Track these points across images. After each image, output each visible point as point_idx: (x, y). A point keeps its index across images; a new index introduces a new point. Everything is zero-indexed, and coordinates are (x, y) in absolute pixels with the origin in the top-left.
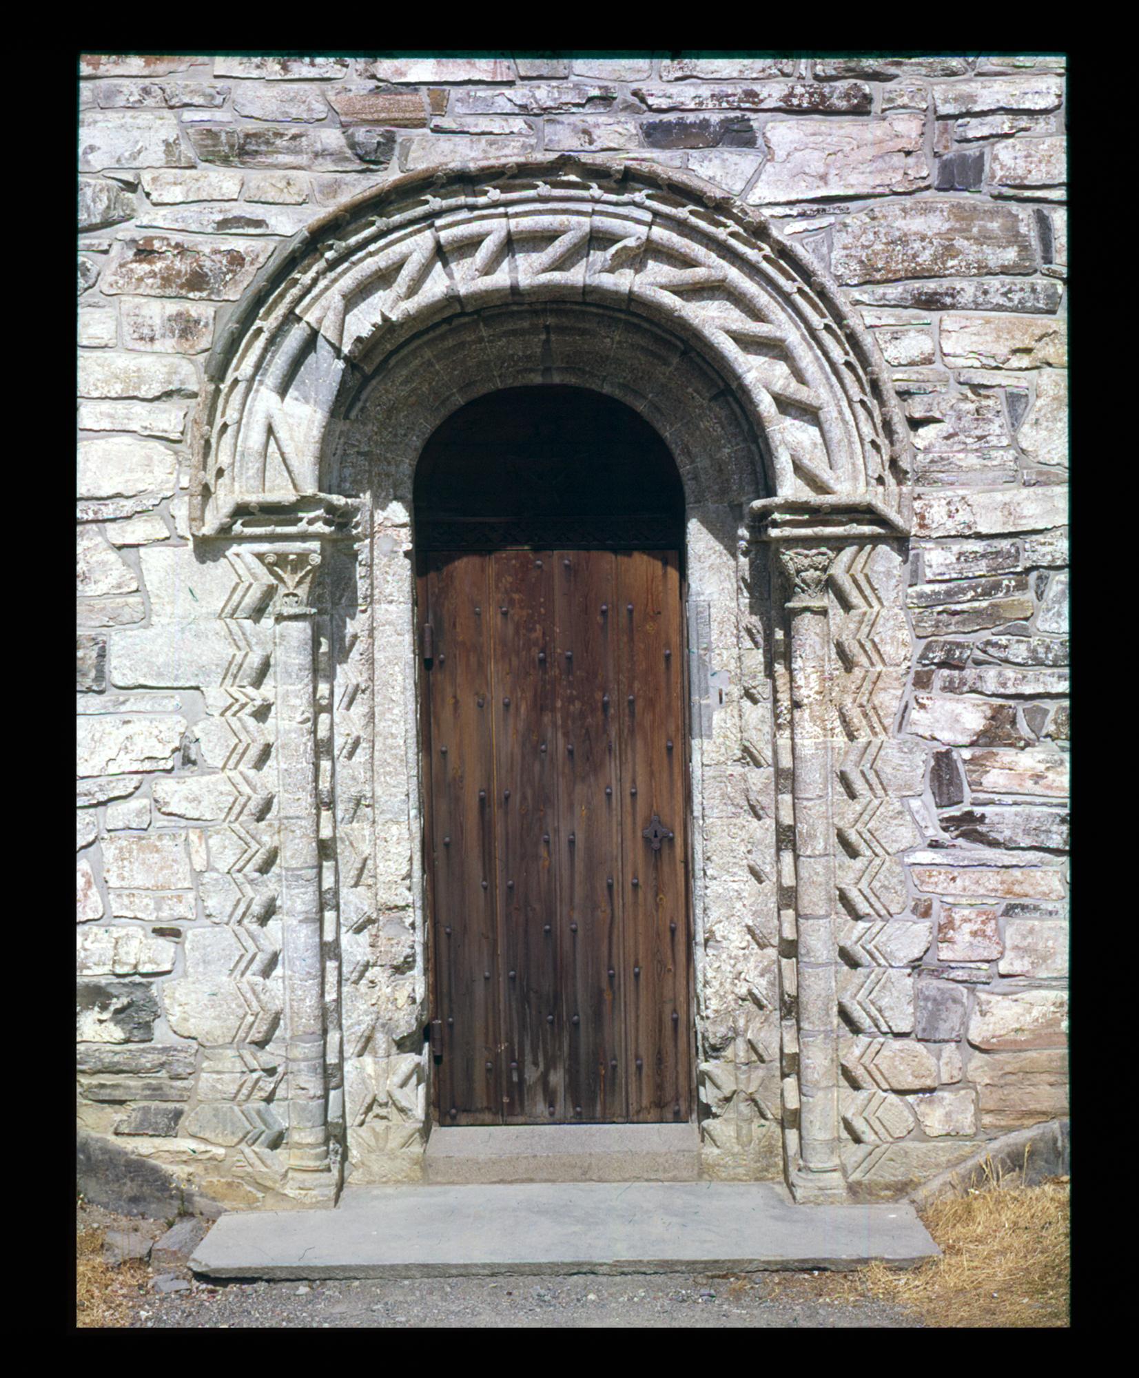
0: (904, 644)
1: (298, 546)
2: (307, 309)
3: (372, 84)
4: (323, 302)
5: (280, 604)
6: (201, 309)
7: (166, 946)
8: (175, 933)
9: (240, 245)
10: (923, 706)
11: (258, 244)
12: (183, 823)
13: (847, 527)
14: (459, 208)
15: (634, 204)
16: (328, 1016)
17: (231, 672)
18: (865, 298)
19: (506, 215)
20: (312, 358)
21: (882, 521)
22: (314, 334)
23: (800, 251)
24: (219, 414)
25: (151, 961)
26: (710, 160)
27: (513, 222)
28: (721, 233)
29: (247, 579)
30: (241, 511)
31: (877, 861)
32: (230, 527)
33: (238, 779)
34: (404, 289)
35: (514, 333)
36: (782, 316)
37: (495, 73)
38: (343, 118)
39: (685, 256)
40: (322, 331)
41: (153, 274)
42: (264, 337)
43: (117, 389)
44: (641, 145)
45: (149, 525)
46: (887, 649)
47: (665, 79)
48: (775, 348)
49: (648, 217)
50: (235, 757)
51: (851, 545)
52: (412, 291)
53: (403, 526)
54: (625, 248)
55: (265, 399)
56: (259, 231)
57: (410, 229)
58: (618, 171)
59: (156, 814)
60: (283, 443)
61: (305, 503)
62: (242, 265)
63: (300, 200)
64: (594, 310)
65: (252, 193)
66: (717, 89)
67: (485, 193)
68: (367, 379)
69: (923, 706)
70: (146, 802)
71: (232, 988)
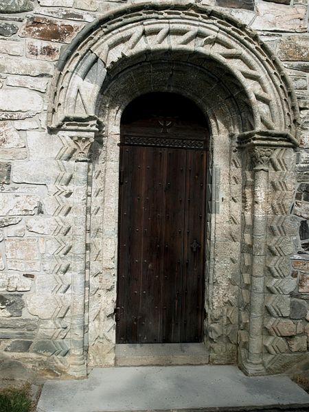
0: (294, 184)
2: (96, 48)
5: (76, 156)
6: (55, 45)
7: (28, 280)
8: (32, 276)
9: (72, 24)
10: (298, 205)
12: (37, 235)
15: (213, 24)
16: (86, 307)
17: (58, 179)
19: (169, 23)
20: (95, 65)
21: (290, 140)
22: (97, 58)
23: (269, 46)
24: (67, 65)
25: (22, 286)
28: (242, 37)
29: (66, 145)
30: (67, 119)
31: (282, 258)
33: (58, 219)
39: (227, 44)
41: (38, 31)
42: (80, 56)
43: (22, 71)
45: (31, 123)
46: (289, 185)
48: (255, 78)
49: (217, 29)
50: (58, 211)
55: (77, 80)
56: (80, 19)
57: (134, 24)
59: (27, 232)
60: (83, 97)
61: (91, 118)
64: (189, 65)
69: (298, 205)
70: (22, 227)
71: (51, 297)
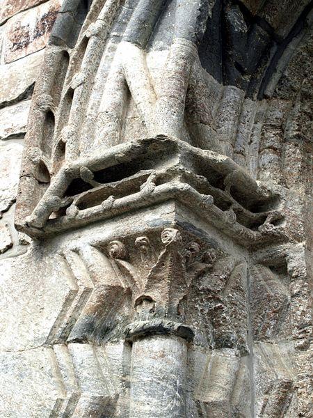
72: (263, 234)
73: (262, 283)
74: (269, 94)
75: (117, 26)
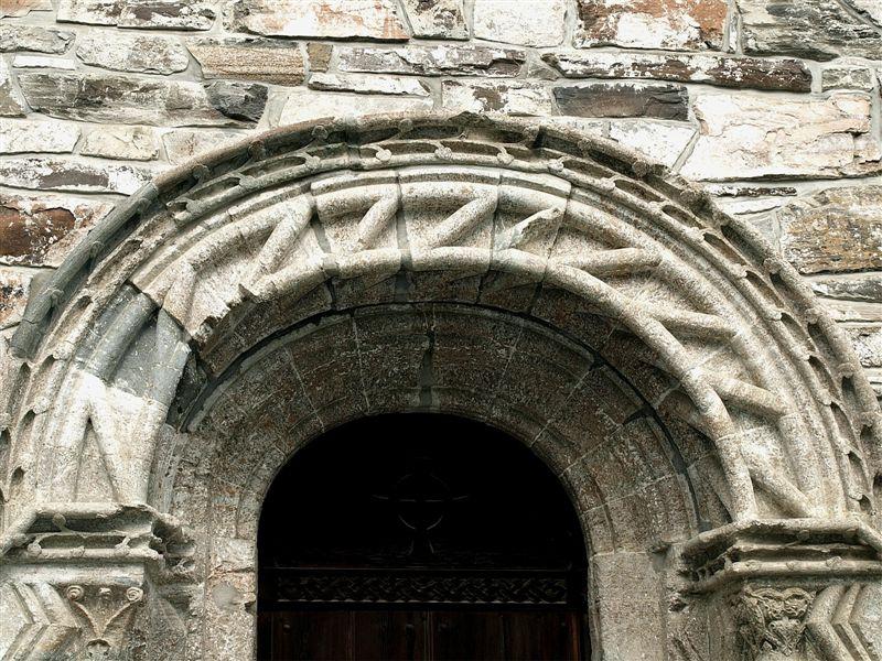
1: (115, 575)
3: (243, 37)
4: (168, 271)
9: (71, 203)
11: (91, 203)
13: (830, 561)
14: (341, 168)
15: (550, 171)
18: (824, 289)
19: (397, 180)
22: (155, 310)
26: (636, 130)
27: (406, 187)
28: (654, 208)
29: (41, 619)
30: (42, 524)
32: (25, 546)
34: (270, 260)
35: (390, 339)
36: (729, 307)
37: (386, 31)
38: (205, 70)
40: (164, 307)
44: (554, 113)
47: (579, 45)
49: (566, 187)
51: (835, 583)
52: (278, 264)
53: (247, 570)
54: (540, 219)
55: (87, 388)
57: (280, 191)
58: (532, 132)
61: (129, 516)
62: (71, 227)
63: (150, 156)
65: (94, 148)
66: (639, 59)
67: (373, 153)
68: (213, 382)
72: (176, 575)
73: (165, 617)
74: (191, 430)
75: (83, 351)
